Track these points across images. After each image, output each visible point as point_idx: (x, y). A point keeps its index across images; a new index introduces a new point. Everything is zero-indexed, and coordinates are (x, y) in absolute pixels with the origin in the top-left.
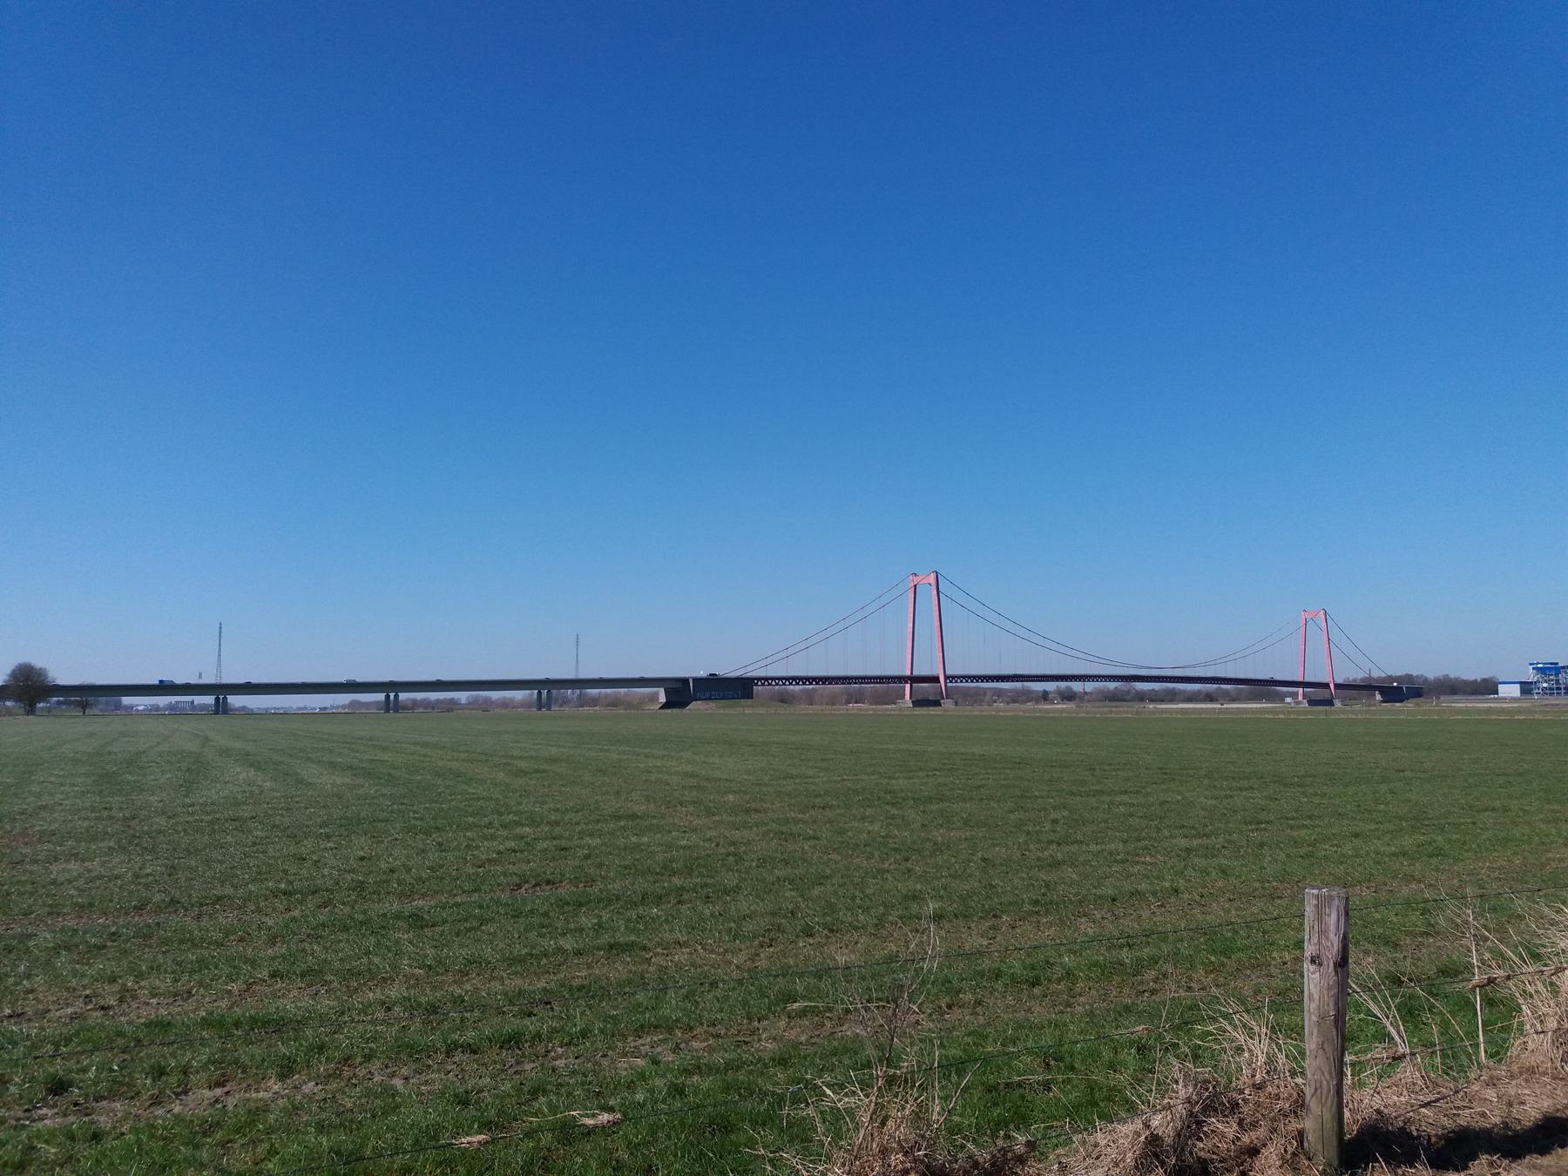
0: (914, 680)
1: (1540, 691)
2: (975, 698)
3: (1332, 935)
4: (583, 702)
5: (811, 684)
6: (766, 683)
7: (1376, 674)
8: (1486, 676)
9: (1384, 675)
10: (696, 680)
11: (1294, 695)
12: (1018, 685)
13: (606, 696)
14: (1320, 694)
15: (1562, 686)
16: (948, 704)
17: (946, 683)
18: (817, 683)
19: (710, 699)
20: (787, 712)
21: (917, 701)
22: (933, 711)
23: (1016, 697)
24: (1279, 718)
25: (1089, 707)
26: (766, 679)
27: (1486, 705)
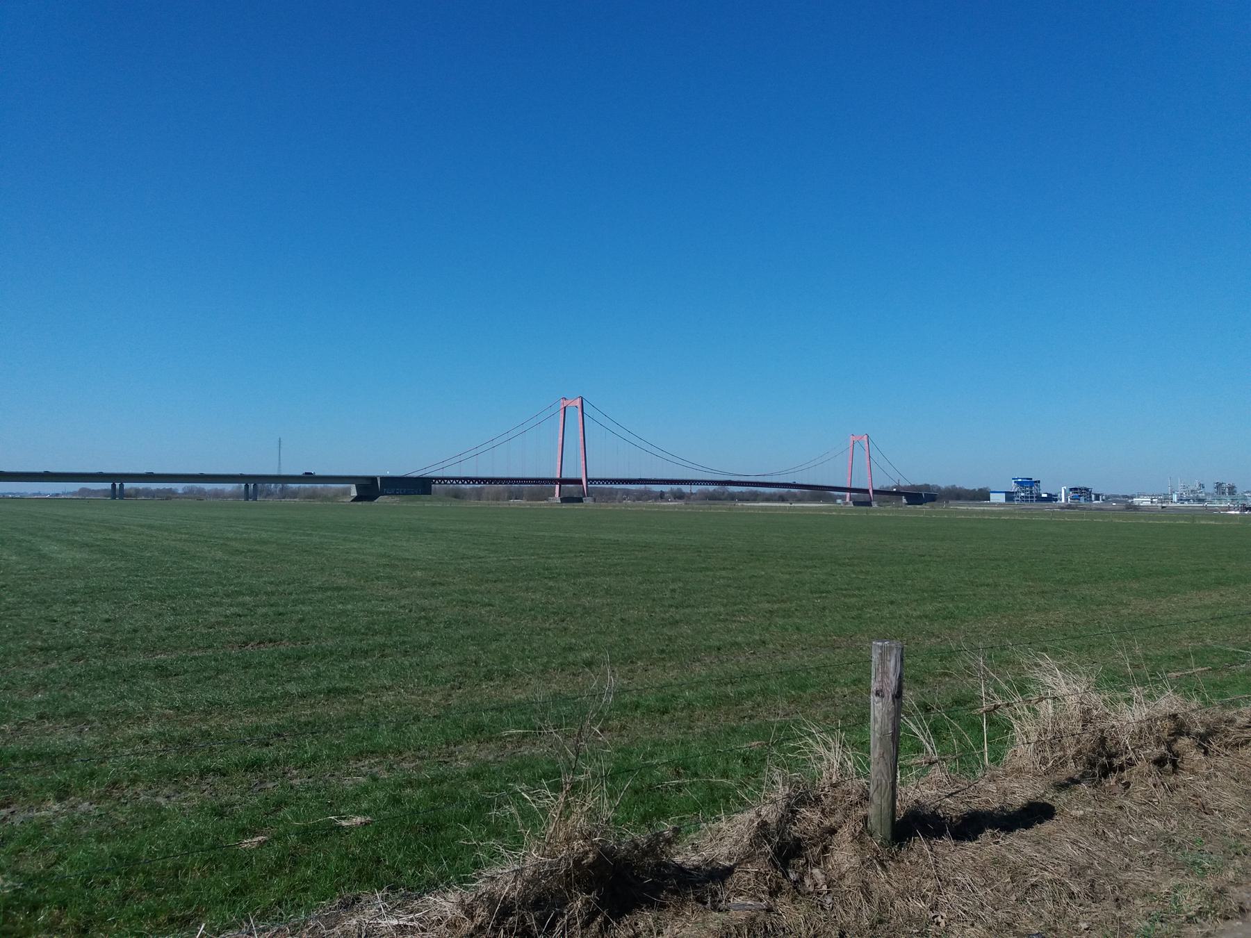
0: (562, 481)
1: (1019, 499)
2: (610, 496)
4: (284, 494)
5: (479, 483)
7: (903, 483)
10: (383, 479)
11: (843, 498)
12: (642, 486)
13: (305, 489)
14: (862, 497)
15: (1034, 496)
16: (588, 501)
17: (587, 484)
18: (485, 483)
19: (395, 494)
22: (577, 506)
23: (640, 496)
26: (443, 479)
27: (982, 508)
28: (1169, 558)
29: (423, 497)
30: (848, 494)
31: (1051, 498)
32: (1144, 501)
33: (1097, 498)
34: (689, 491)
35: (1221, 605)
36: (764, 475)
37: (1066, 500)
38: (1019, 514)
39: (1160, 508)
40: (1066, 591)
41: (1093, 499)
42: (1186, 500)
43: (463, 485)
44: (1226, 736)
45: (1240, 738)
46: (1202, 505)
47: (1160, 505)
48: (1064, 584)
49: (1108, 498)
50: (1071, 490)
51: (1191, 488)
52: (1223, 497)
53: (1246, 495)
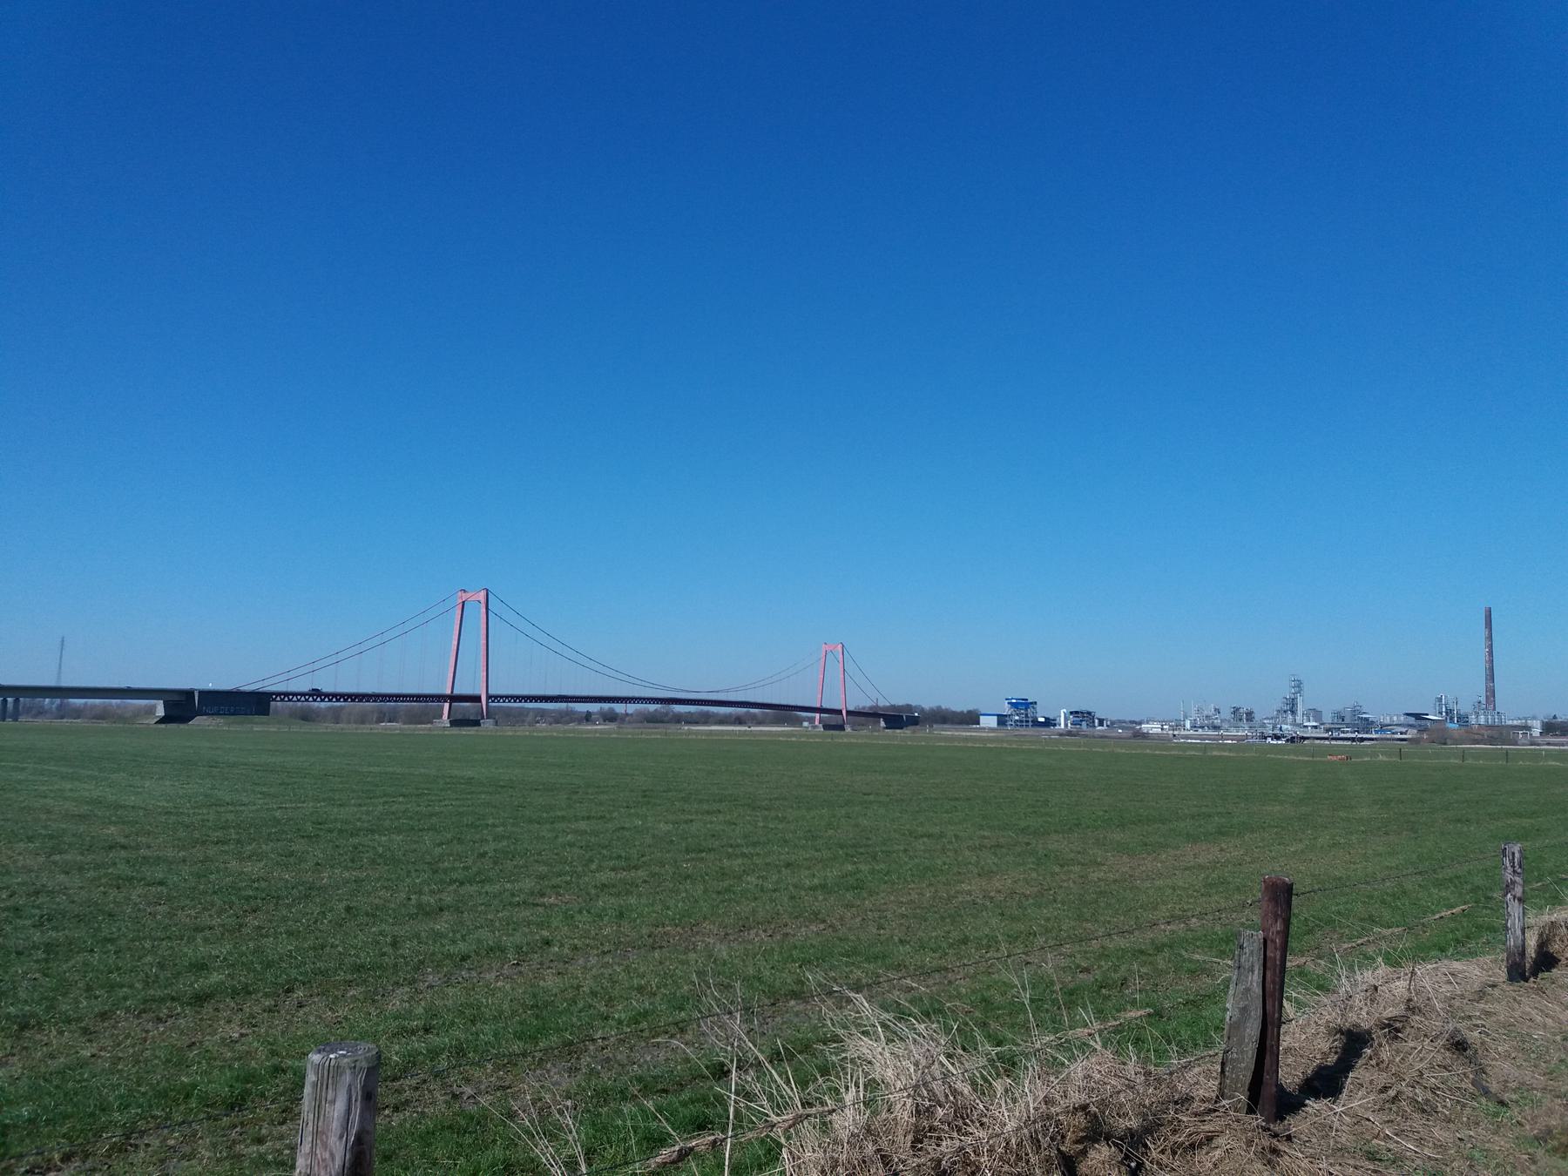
0: (454, 698)
2: (517, 718)
3: (333, 1140)
4: (62, 713)
5: (338, 701)
6: (286, 699)
7: (882, 703)
8: (971, 708)
9: (888, 704)
10: (203, 693)
11: (811, 720)
12: (563, 706)
13: (94, 707)
14: (834, 720)
15: (1030, 720)
16: (487, 724)
17: (487, 702)
18: (345, 700)
19: (218, 714)
20: (302, 730)
21: (455, 720)
22: (471, 731)
23: (560, 718)
24: (791, 741)
25: (629, 731)
26: (287, 694)
27: (968, 734)
28: (1168, 799)
29: (257, 718)
30: (817, 715)
31: (1049, 723)
32: (1153, 728)
33: (1101, 723)
34: (623, 712)
35: (1218, 865)
36: (718, 692)
37: (1066, 725)
38: (1007, 742)
39: (1171, 736)
40: (1028, 844)
41: (1096, 724)
42: (1200, 727)
43: (316, 704)
44: (1174, 1132)
45: (1198, 1133)
46: (1217, 733)
47: (1171, 732)
48: (1029, 835)
49: (1113, 723)
50: (1071, 713)
51: (1206, 713)
52: (1240, 724)
53: (1265, 721)
